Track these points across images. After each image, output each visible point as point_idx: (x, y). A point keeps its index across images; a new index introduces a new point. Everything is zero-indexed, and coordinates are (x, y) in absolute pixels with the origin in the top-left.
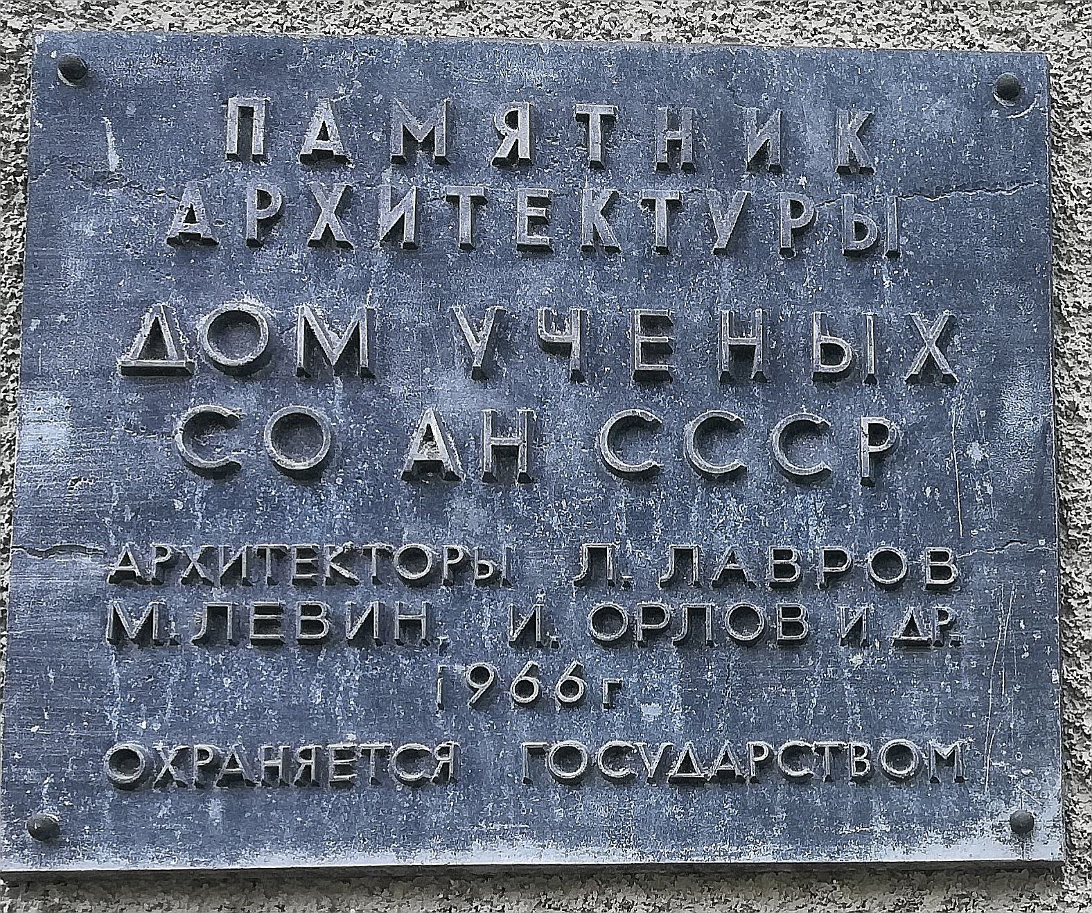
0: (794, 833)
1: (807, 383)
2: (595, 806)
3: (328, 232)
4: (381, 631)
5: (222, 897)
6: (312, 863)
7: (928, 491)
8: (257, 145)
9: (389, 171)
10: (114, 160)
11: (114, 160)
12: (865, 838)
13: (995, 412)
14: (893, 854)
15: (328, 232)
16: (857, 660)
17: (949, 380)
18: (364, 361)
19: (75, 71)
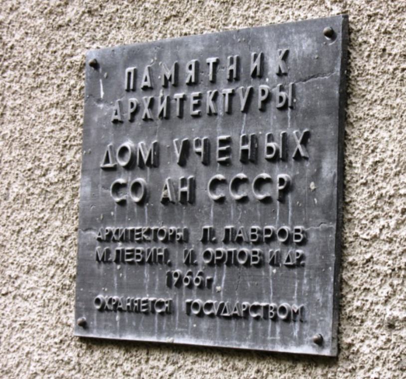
0: (255, 339)
1: (265, 161)
2: (205, 324)
3: (146, 116)
4: (190, 198)
5: (169, 352)
6: (137, 339)
7: (298, 202)
8: (131, 87)
9: (161, 90)
10: (102, 94)
11: (102, 94)
12: (273, 342)
13: (319, 169)
14: (280, 349)
15: (146, 116)
16: (275, 271)
17: (306, 158)
18: (152, 162)
19: (95, 65)
